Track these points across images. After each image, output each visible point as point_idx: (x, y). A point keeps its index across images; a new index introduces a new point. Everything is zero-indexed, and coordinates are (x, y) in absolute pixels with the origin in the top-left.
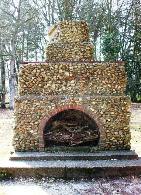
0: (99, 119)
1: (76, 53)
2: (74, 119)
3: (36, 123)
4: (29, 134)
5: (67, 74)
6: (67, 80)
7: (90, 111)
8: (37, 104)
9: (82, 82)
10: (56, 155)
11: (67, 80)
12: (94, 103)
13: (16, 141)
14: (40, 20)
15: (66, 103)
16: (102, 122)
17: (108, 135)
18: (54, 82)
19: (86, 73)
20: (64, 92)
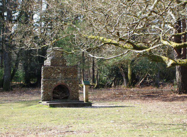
0: (70, 88)
1: (61, 62)
2: (149, 96)
3: (50, 90)
4: (48, 94)
5: (59, 71)
6: (59, 73)
7: (67, 85)
8: (51, 82)
9: (64, 74)
10: (58, 101)
11: (59, 73)
12: (68, 82)
13: (43, 97)
14: (120, 90)
15: (60, 82)
16: (70, 89)
17: (73, 94)
18: (55, 74)
19: (65, 70)
20: (58, 78)
